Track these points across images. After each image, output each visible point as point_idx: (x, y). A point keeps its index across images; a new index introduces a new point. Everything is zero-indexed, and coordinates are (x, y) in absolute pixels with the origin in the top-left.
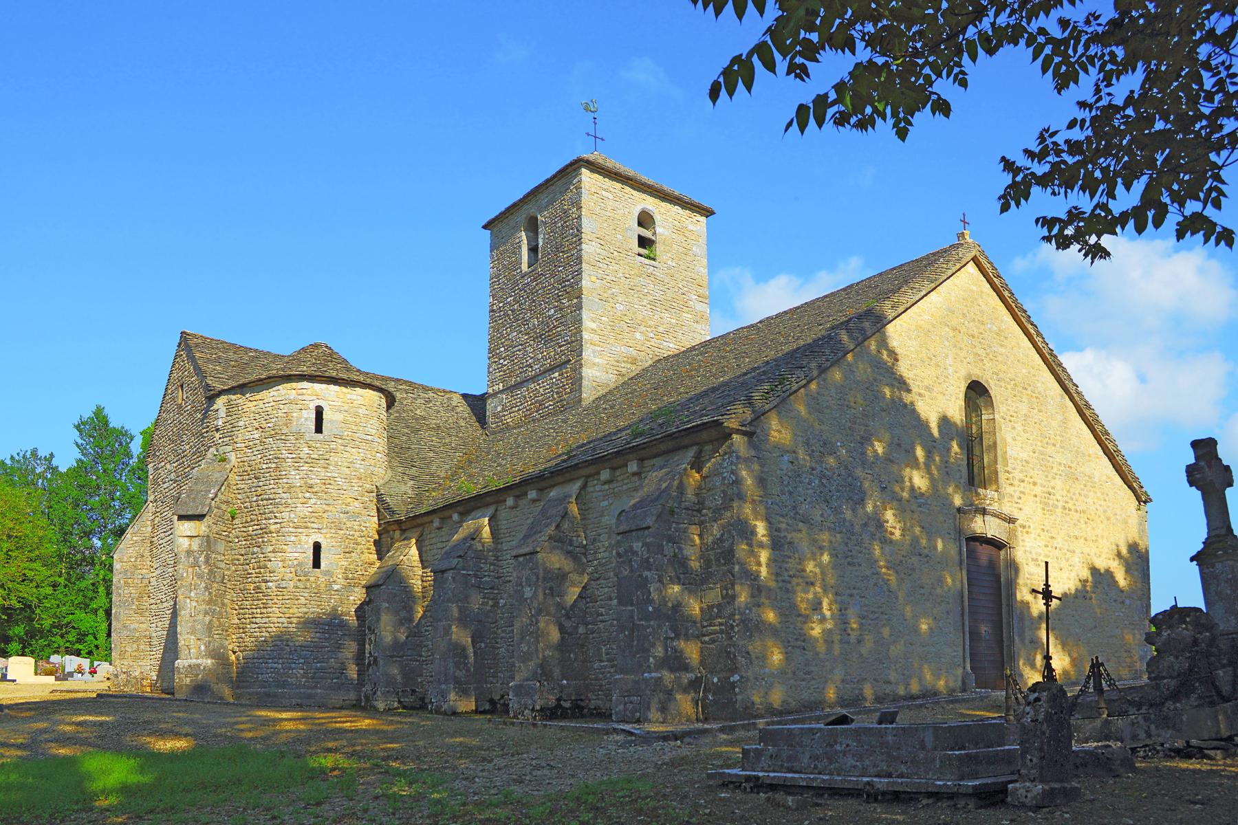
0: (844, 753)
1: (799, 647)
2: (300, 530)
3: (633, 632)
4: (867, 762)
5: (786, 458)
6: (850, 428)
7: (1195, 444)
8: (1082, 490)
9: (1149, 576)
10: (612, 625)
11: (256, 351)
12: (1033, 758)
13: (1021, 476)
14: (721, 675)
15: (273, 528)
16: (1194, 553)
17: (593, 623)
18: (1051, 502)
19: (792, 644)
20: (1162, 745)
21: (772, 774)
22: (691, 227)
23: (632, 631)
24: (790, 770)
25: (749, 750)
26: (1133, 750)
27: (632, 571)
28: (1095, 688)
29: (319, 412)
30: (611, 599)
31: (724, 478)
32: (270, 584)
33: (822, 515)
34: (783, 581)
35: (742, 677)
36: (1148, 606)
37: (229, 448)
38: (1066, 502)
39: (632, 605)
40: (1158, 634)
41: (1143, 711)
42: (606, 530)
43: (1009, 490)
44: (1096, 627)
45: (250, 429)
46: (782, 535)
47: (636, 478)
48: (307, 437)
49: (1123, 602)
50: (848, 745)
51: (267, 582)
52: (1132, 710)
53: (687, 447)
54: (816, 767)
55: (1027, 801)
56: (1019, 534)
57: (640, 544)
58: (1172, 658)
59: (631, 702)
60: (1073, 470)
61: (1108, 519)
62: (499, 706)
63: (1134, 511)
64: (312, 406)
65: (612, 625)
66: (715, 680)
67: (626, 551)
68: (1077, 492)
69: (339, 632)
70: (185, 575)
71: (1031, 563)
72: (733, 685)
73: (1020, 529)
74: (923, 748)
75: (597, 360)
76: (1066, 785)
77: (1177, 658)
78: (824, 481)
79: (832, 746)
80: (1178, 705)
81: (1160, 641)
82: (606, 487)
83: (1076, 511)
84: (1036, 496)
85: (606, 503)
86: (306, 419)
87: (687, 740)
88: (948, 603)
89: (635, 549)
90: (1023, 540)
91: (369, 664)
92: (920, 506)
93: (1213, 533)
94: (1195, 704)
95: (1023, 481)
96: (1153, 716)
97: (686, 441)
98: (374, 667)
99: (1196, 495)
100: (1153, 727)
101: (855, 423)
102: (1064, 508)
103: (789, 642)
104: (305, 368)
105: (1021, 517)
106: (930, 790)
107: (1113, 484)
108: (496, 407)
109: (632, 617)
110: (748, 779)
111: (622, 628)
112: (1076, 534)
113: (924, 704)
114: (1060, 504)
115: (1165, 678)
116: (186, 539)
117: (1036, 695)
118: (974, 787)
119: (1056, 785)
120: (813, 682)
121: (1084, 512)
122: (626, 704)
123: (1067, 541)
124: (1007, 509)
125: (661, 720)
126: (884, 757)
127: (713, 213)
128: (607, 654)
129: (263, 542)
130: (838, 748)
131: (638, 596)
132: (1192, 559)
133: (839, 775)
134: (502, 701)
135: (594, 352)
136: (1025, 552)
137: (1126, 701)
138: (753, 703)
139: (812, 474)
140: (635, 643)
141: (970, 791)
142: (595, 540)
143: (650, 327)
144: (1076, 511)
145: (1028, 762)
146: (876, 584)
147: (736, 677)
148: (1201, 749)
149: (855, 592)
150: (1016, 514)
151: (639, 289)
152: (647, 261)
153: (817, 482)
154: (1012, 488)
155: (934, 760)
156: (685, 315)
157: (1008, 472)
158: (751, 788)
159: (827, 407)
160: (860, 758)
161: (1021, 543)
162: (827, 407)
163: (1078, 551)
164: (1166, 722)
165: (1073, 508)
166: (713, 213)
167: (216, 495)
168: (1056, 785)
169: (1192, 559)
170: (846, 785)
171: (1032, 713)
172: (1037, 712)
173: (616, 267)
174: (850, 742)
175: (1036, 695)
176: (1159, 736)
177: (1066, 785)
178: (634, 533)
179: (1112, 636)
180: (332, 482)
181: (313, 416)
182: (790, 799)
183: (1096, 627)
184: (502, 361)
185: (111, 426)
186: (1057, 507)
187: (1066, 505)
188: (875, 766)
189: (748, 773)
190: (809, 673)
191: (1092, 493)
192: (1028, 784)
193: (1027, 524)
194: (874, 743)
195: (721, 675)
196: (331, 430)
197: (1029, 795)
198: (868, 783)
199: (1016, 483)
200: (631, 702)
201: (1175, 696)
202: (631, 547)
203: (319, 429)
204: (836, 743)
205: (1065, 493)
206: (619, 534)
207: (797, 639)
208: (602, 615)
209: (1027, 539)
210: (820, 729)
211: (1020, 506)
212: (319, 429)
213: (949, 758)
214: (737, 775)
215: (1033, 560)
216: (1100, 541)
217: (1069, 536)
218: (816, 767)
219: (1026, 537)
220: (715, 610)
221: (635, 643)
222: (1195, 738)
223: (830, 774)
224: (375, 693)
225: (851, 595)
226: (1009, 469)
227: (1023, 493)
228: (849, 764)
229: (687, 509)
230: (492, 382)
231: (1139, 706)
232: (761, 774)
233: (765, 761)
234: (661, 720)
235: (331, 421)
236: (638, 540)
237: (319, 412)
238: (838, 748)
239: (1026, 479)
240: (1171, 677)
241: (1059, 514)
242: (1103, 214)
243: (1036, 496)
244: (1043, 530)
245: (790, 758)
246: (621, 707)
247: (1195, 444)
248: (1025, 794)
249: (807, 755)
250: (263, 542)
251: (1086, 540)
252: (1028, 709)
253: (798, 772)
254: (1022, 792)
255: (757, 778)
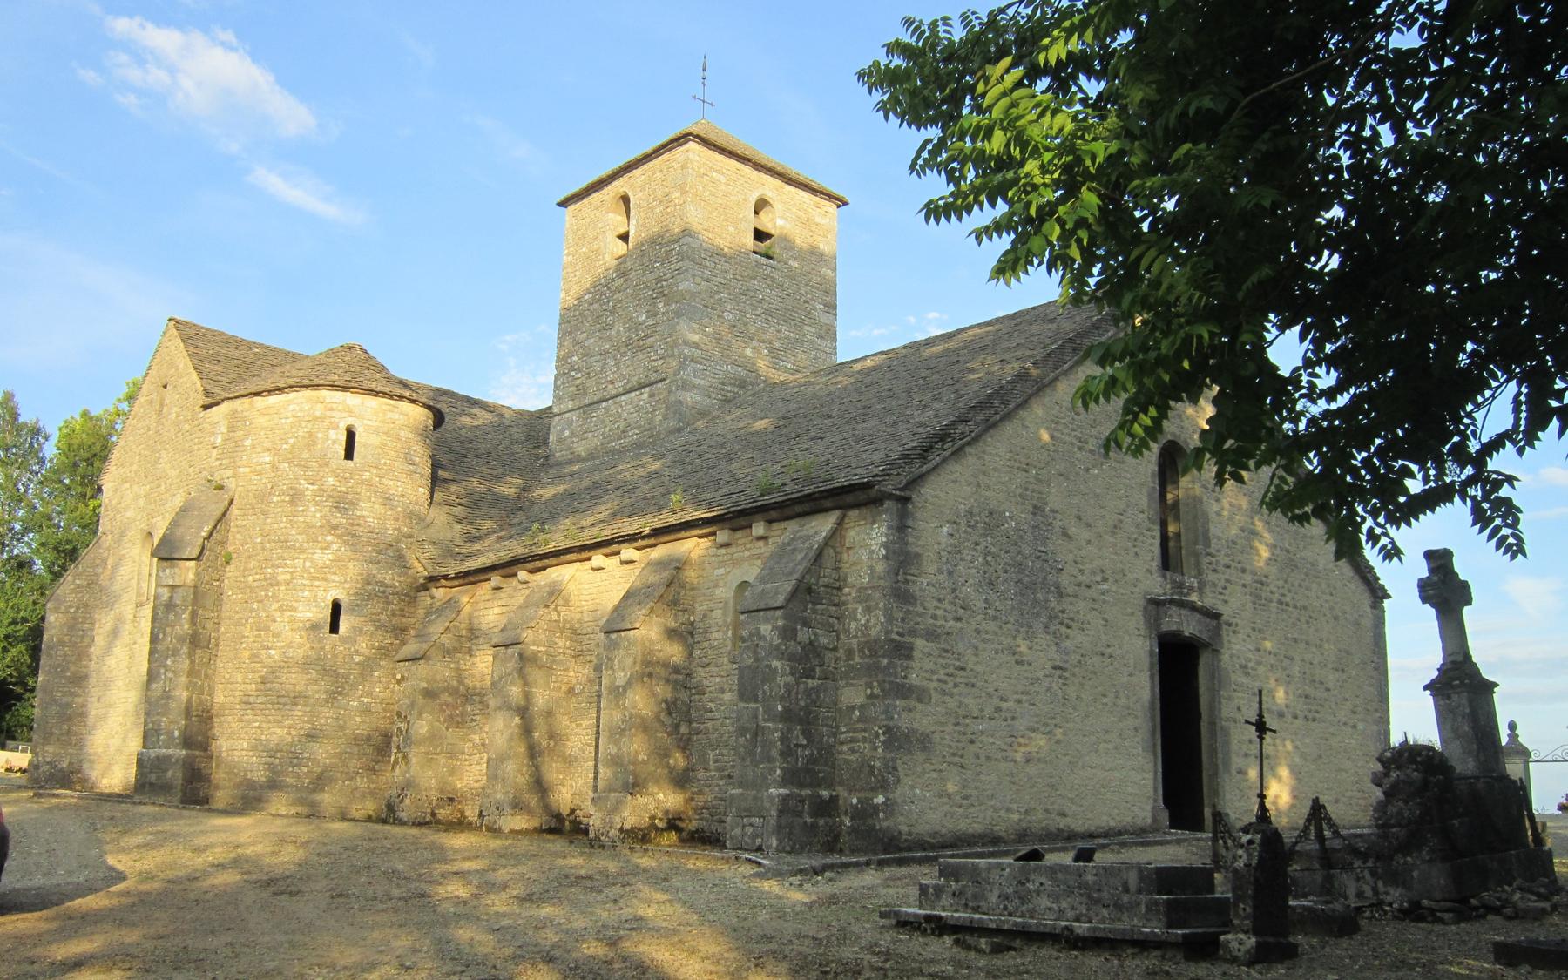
0: (1038, 893)
1: (955, 764)
2: (317, 583)
3: (756, 735)
4: (1064, 904)
5: (945, 529)
6: (1020, 495)
7: (1429, 555)
8: (1304, 580)
9: (1387, 693)
10: (723, 725)
11: (261, 346)
12: (1245, 908)
13: (1227, 560)
14: (863, 795)
15: (281, 578)
16: (1427, 681)
17: (699, 721)
18: (1264, 595)
19: (947, 759)
20: (1390, 905)
21: (956, 915)
22: (818, 220)
23: (756, 735)
24: (976, 910)
25: (927, 886)
26: (1359, 909)
27: (757, 660)
28: (1316, 836)
29: (351, 436)
30: (723, 691)
31: (872, 552)
32: (272, 652)
33: (986, 601)
34: (939, 680)
35: (887, 799)
36: (1387, 733)
37: (229, 473)
38: (1283, 595)
39: (756, 701)
40: (1386, 775)
41: (1370, 864)
42: (720, 605)
43: (1211, 577)
44: (1320, 757)
45: (259, 450)
46: (939, 623)
47: (761, 543)
48: (334, 464)
49: (1354, 727)
50: (1042, 884)
51: (268, 648)
52: (1357, 863)
53: (827, 510)
54: (1005, 908)
55: (1240, 954)
56: (1224, 633)
57: (770, 627)
58: (1401, 804)
59: (751, 825)
60: (1291, 555)
61: (1336, 618)
62: (567, 823)
63: (1368, 610)
64: (343, 426)
65: (723, 725)
66: (855, 801)
67: (751, 635)
68: (1296, 583)
69: (358, 719)
70: (161, 636)
71: (1239, 672)
72: (876, 808)
73: (1224, 627)
74: (1126, 890)
75: (697, 381)
76: (1282, 940)
77: (1406, 802)
78: (989, 559)
79: (1023, 884)
80: (1409, 859)
81: (1387, 783)
82: (723, 551)
83: (1295, 607)
84: (1244, 586)
85: (721, 571)
86: (334, 442)
87: (828, 874)
88: (1136, 717)
89: (763, 633)
90: (1229, 642)
91: (396, 762)
92: (1103, 594)
93: (1451, 659)
94: (1427, 858)
95: (1229, 567)
96: (1380, 871)
97: (828, 504)
98: (403, 767)
99: (1429, 612)
100: (1380, 884)
101: (1026, 489)
102: (1280, 602)
103: (944, 757)
104: (336, 377)
105: (1226, 611)
106: (1135, 937)
107: (1342, 574)
108: (562, 431)
109: (756, 717)
110: (928, 918)
111: (742, 731)
112: (1296, 636)
113: (1108, 845)
114: (1276, 597)
115: (1393, 826)
116: (166, 589)
117: (1249, 837)
118: (1184, 935)
119: (1271, 940)
120: (972, 810)
121: (1305, 608)
122: (744, 826)
123: (1283, 644)
124: (1209, 601)
125: (788, 848)
126: (1084, 899)
127: (845, 203)
128: (716, 761)
129: (266, 596)
130: (1030, 886)
131: (764, 693)
132: (1426, 688)
133: (1032, 917)
134: (572, 818)
135: (694, 372)
136: (1231, 657)
137: (1355, 850)
138: (900, 833)
139: (975, 550)
140: (759, 749)
141: (1180, 940)
142: (705, 616)
143: (764, 342)
144: (1295, 607)
145: (1241, 912)
146: (1049, 689)
147: (880, 799)
148: (1432, 911)
149: (1025, 698)
150: (1221, 609)
151: (752, 294)
152: (763, 260)
153: (980, 559)
154: (1216, 576)
155: (1139, 904)
156: (806, 328)
157: (1209, 554)
158: (932, 929)
159: (995, 469)
160: (1057, 900)
161: (1226, 645)
162: (995, 469)
163: (1297, 658)
164: (1394, 878)
165: (1291, 603)
166: (845, 203)
167: (211, 534)
168: (1271, 940)
169: (1426, 688)
170: (1041, 929)
171: (1245, 857)
172: (1249, 855)
173: (726, 267)
174: (1043, 880)
175: (1249, 837)
176: (1387, 893)
177: (1282, 940)
178: (762, 613)
179: (1340, 770)
180: (362, 522)
181: (343, 438)
182: (983, 941)
183: (1320, 757)
184: (573, 374)
185: (21, 420)
186: (1271, 601)
187: (1283, 599)
188: (1073, 908)
189: (928, 912)
190: (966, 798)
191: (1314, 585)
192: (1241, 936)
193: (1234, 621)
194: (1071, 883)
195: (863, 795)
196: (365, 456)
197: (1243, 948)
198: (1066, 927)
199: (1220, 568)
200: (751, 825)
201: (1405, 848)
202: (758, 630)
203: (349, 454)
204: (1028, 881)
205: (1281, 583)
206: (743, 613)
207: (954, 755)
208: (711, 711)
209: (1233, 640)
210: (1010, 864)
211: (1226, 598)
212: (349, 454)
213: (1156, 903)
214: (915, 915)
215: (1241, 666)
216: (1326, 646)
217: (1286, 639)
218: (1005, 908)
219: (1233, 638)
220: (857, 713)
221: (759, 749)
222: (1427, 898)
223: (1022, 916)
224: (402, 801)
225: (1019, 702)
226: (1211, 550)
227: (1227, 581)
228: (1043, 906)
229: (826, 586)
230: (558, 398)
231: (1364, 856)
232: (943, 914)
233: (946, 900)
234: (788, 848)
235: (365, 446)
236: (767, 620)
237: (351, 436)
238: (1030, 886)
239: (1233, 564)
240: (1399, 825)
241: (1274, 610)
242: (1297, 511)
243: (1244, 586)
244: (1254, 629)
245: (975, 897)
246: (738, 831)
247: (1429, 555)
248: (1237, 946)
249: (996, 893)
250: (266, 596)
251: (1307, 644)
252: (1240, 852)
253: (984, 913)
254: (1234, 945)
255: (940, 918)
